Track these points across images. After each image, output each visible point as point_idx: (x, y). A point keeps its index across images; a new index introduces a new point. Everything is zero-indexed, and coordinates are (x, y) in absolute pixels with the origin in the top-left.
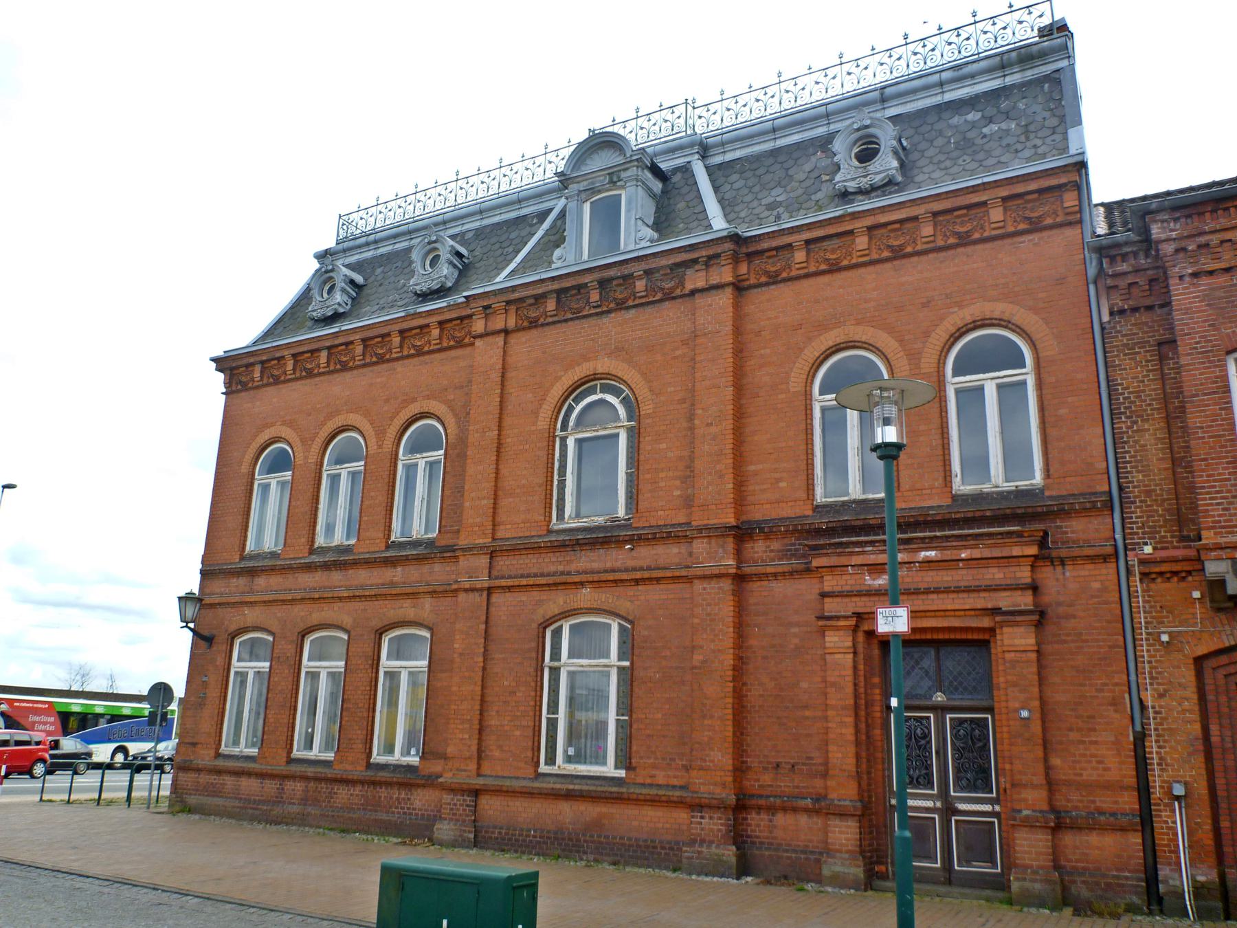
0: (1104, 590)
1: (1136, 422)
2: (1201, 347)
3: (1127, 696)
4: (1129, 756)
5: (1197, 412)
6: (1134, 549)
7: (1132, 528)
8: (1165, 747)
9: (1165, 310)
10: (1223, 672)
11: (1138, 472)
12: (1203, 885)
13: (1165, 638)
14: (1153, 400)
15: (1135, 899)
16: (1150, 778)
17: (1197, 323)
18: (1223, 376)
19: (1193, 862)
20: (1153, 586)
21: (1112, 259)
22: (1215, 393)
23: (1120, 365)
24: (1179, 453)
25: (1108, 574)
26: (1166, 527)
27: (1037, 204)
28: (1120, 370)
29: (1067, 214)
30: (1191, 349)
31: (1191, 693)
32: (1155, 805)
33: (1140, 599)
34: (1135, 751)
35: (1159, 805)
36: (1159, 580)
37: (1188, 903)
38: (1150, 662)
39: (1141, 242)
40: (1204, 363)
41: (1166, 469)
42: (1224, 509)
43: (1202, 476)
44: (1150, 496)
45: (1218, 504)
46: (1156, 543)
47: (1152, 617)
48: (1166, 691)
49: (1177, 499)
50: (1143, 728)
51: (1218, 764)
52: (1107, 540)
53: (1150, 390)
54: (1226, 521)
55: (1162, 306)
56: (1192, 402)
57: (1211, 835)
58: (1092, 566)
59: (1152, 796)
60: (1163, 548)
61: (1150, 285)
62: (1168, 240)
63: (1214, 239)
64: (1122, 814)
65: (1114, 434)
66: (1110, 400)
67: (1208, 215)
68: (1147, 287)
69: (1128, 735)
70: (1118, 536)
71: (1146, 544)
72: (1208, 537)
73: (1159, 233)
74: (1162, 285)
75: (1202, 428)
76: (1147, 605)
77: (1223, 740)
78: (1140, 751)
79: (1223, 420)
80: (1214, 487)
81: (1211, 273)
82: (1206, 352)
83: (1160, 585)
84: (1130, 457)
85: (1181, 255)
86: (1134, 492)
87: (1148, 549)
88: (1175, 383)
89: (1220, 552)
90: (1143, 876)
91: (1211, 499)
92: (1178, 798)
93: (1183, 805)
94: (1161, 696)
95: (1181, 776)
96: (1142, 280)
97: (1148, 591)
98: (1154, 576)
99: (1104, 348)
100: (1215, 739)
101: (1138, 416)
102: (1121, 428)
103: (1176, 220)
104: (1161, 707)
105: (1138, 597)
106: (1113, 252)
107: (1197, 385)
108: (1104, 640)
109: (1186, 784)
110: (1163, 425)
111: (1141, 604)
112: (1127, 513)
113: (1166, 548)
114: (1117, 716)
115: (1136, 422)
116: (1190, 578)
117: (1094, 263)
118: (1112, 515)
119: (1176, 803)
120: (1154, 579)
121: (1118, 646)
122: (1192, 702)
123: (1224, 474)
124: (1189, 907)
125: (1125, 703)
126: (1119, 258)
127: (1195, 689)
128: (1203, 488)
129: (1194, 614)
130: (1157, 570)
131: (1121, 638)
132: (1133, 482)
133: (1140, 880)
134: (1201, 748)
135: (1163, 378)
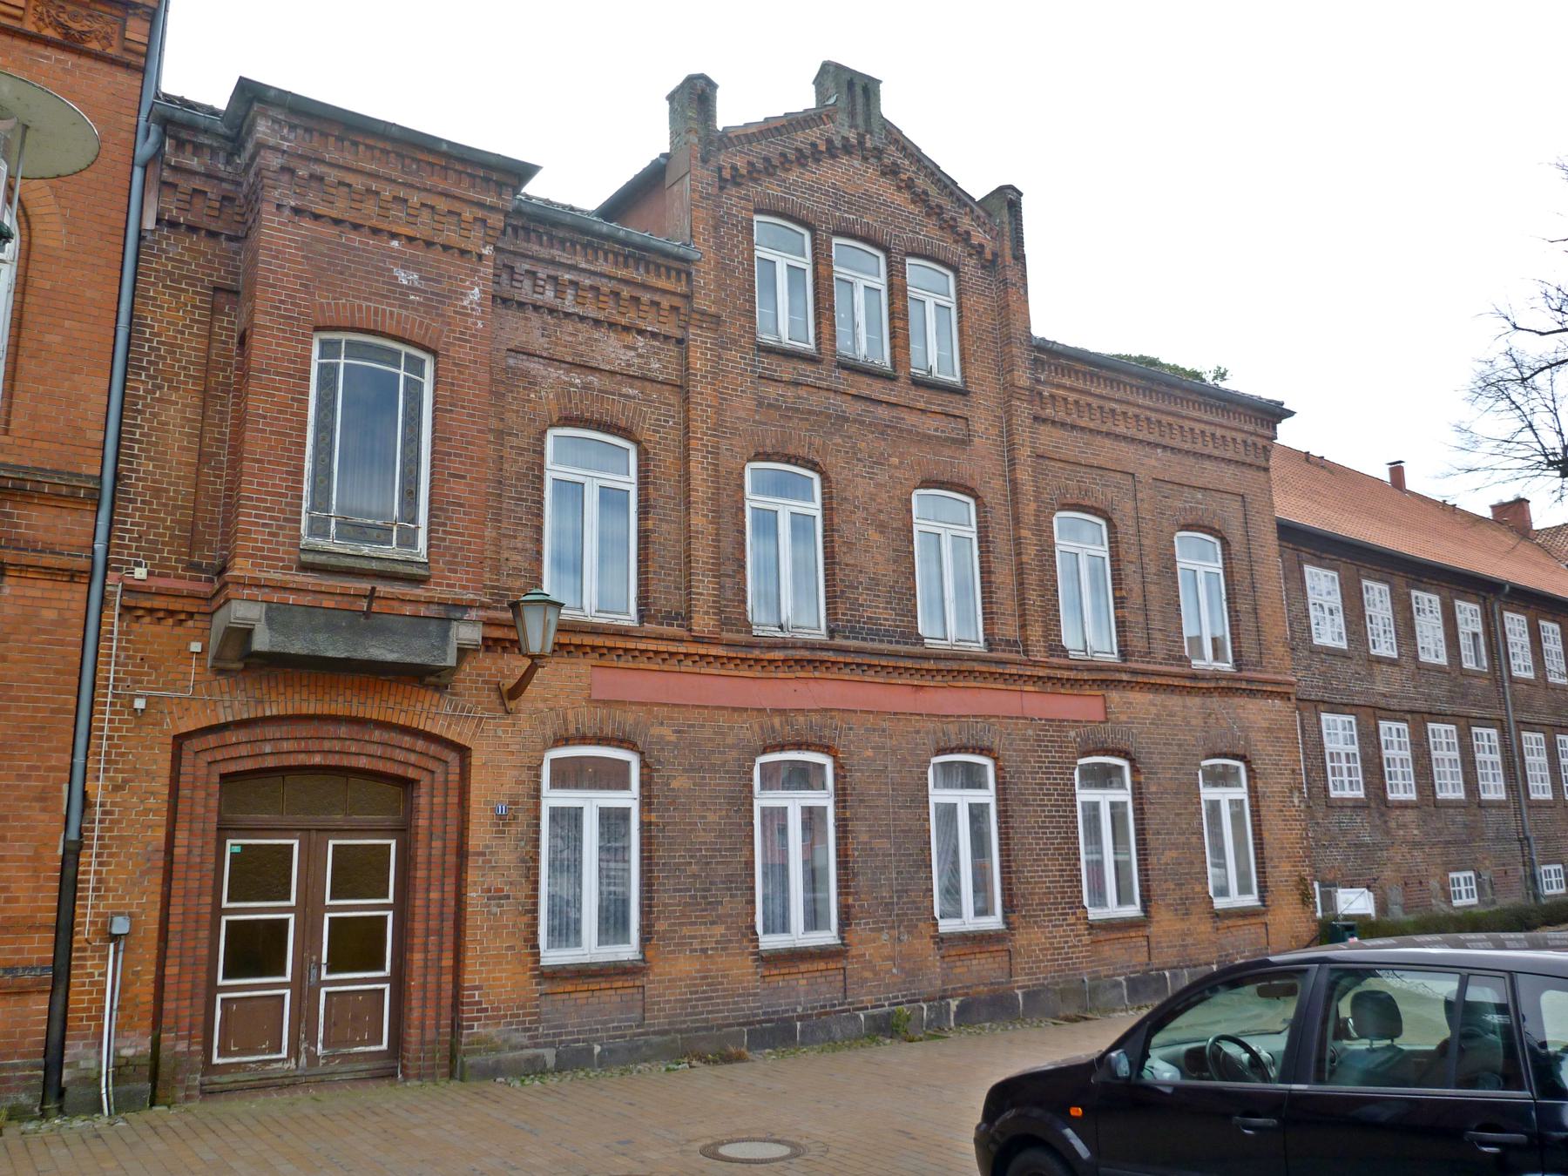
0: (62, 622)
1: (160, 388)
2: (286, 310)
3: (65, 787)
4: (49, 878)
5: (261, 394)
6: (118, 570)
7: (123, 538)
8: (109, 864)
9: (235, 245)
10: (208, 757)
11: (149, 458)
12: (128, 1062)
13: (140, 704)
14: (192, 363)
15: (24, 1098)
16: (78, 911)
17: (287, 275)
18: (305, 356)
19: (120, 1030)
20: (136, 627)
21: (180, 145)
22: (290, 376)
23: (155, 299)
24: (211, 447)
25: (73, 599)
26: (172, 545)
27: (84, 13)
28: (153, 306)
29: (126, 49)
30: (271, 307)
31: (161, 786)
32: (78, 950)
33: (115, 644)
34: (62, 870)
35: (84, 950)
36: (147, 619)
37: (104, 1091)
38: (109, 738)
39: (226, 138)
40: (284, 331)
41: (188, 464)
42: (270, 534)
43: (251, 483)
44: (158, 498)
45: (264, 525)
46: (153, 566)
47: (125, 673)
48: (125, 781)
49: (195, 509)
50: (81, 836)
51: (177, 886)
52: (82, 548)
53: (189, 348)
54: (270, 550)
55: (230, 239)
56: (260, 378)
57: (151, 988)
58: (49, 584)
59: (76, 938)
60: (161, 575)
61: (221, 202)
62: (275, 149)
63: (333, 175)
64: (24, 969)
65: (124, 395)
66: (129, 344)
67: (332, 139)
68: (217, 205)
69: (57, 847)
70: (100, 546)
71: (139, 565)
72: (241, 568)
73: (264, 133)
74: (237, 209)
75: (265, 417)
76: (122, 655)
77: (190, 852)
78: (70, 871)
79: (293, 414)
80: (265, 501)
81: (317, 217)
82: (291, 318)
83: (146, 627)
84: (141, 435)
85: (286, 178)
86: (136, 486)
87: (141, 573)
88: (224, 349)
89: (255, 591)
90: (41, 1060)
91: (257, 516)
92: (115, 938)
93: (121, 947)
94: (117, 788)
95: (125, 906)
96: (212, 191)
97: (128, 634)
98: (140, 613)
99: (136, 267)
100: (178, 851)
101: (164, 379)
102: (137, 389)
103: (293, 127)
104: (113, 804)
105: (111, 640)
106: (184, 135)
107: (270, 358)
108: (46, 700)
109: (131, 915)
110: (196, 401)
111: (114, 652)
112: (120, 514)
113: (168, 576)
114: (45, 816)
115: (160, 388)
116: (190, 623)
117: (153, 138)
118: (97, 512)
119: (112, 946)
120: (138, 617)
121: (67, 712)
122: (159, 802)
123: (280, 487)
124: (104, 1097)
125: (60, 798)
126: (189, 148)
127: (167, 781)
128: (251, 499)
129: (186, 674)
130: (148, 604)
131: (73, 699)
132: (137, 471)
133: (35, 1067)
134: (161, 864)
135: (210, 336)
